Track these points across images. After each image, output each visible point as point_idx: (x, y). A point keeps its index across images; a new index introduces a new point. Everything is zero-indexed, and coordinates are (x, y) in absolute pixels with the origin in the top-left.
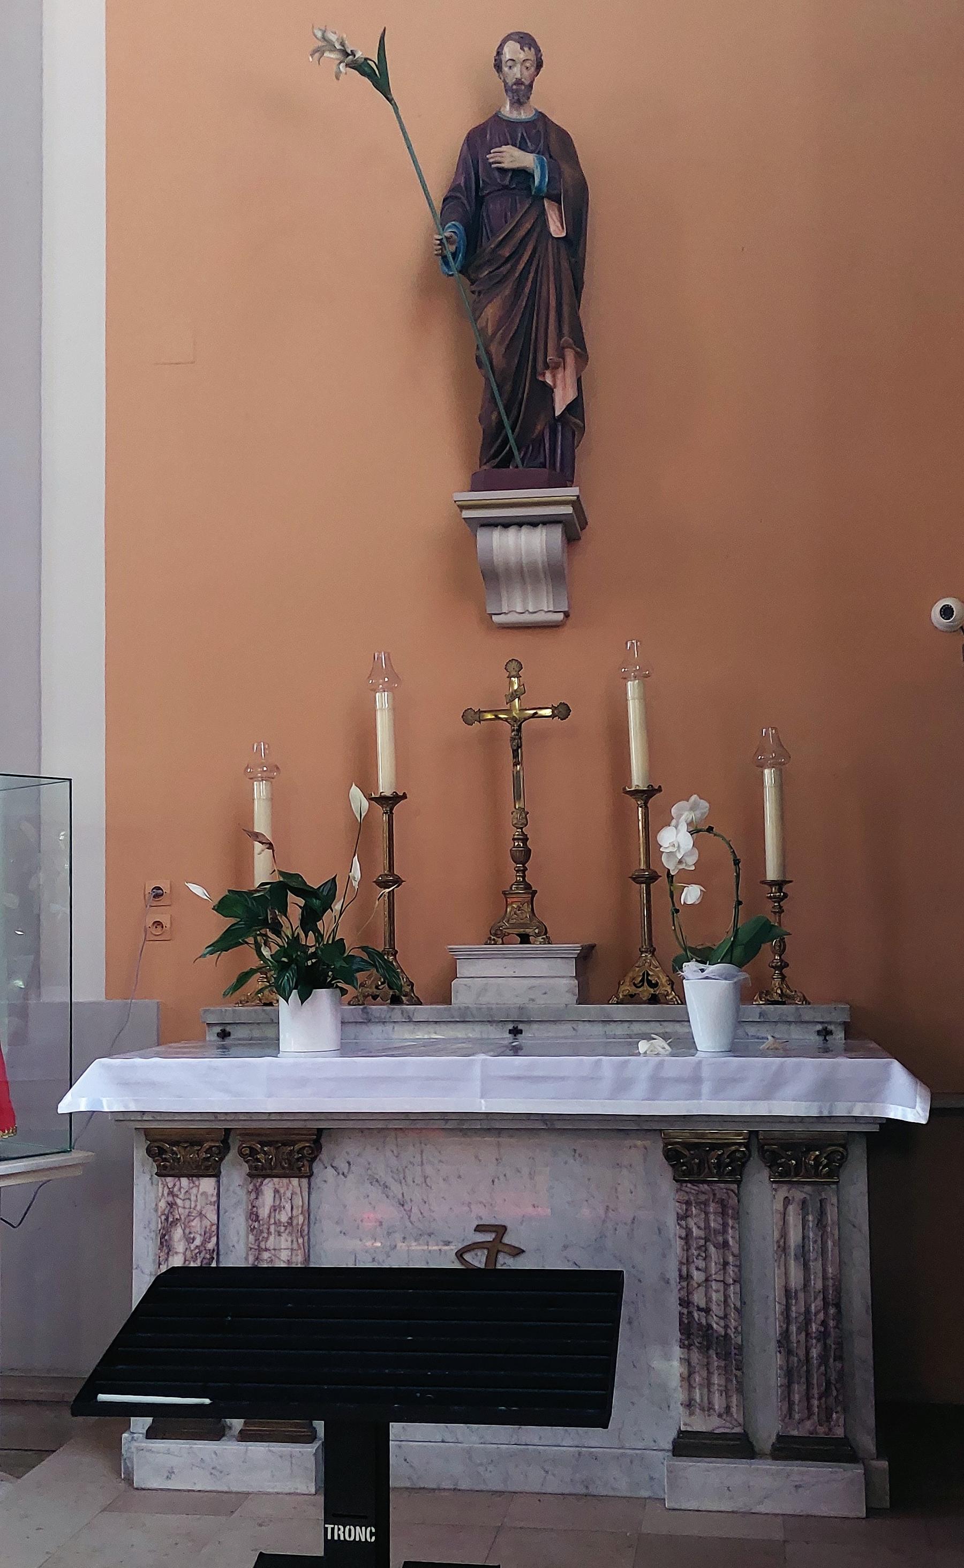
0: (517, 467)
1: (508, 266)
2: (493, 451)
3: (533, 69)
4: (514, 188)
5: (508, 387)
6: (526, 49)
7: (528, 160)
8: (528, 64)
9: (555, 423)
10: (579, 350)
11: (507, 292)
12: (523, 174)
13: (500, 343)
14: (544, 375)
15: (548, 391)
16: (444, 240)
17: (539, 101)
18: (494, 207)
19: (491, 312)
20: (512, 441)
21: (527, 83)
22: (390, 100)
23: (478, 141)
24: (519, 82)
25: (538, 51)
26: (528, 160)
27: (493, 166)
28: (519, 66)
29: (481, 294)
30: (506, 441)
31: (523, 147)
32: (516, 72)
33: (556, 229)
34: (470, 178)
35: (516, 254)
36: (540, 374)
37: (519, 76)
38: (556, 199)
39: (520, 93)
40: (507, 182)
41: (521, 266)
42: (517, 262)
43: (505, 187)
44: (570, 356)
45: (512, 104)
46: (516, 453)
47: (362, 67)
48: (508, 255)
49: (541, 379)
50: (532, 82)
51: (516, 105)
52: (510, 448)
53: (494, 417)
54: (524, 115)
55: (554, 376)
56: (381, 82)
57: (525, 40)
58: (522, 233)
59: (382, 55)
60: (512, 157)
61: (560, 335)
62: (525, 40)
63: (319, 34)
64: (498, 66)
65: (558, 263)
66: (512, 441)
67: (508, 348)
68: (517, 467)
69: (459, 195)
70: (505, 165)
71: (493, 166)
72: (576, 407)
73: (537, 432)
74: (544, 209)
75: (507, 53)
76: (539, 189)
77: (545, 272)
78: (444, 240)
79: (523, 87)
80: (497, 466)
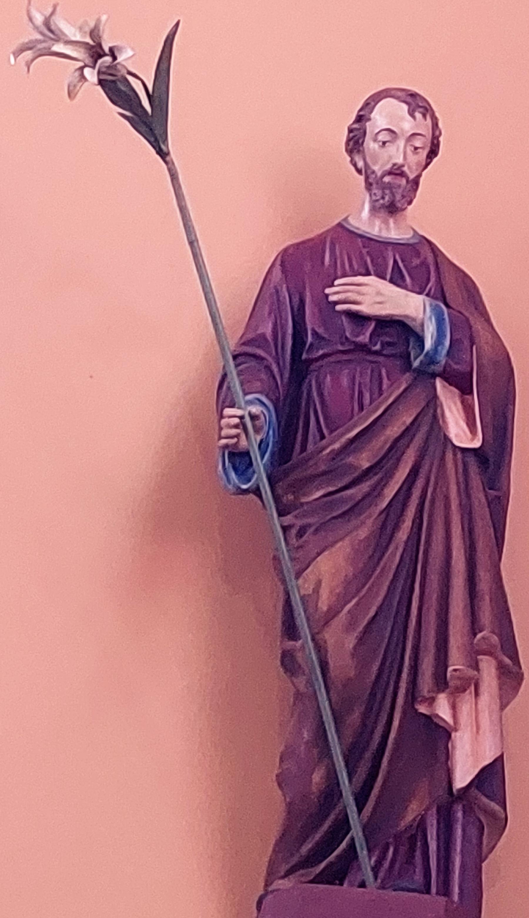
0: (363, 885)
1: (365, 487)
2: (305, 849)
3: (424, 154)
4: (376, 353)
5: (355, 717)
6: (418, 115)
7: (412, 305)
8: (418, 144)
9: (450, 802)
10: (507, 661)
11: (363, 533)
12: (398, 330)
13: (350, 626)
14: (431, 701)
15: (437, 737)
16: (248, 420)
17: (425, 218)
18: (333, 383)
19: (330, 568)
20: (356, 831)
21: (412, 176)
22: (163, 154)
23: (305, 267)
24: (397, 171)
25: (435, 125)
26: (412, 305)
27: (339, 307)
28: (401, 143)
29: (304, 539)
30: (343, 825)
31: (397, 280)
32: (396, 154)
33: (460, 431)
34: (284, 327)
35: (383, 466)
36: (425, 700)
37: (400, 160)
38: (462, 384)
39: (394, 192)
40: (364, 338)
41: (390, 492)
42: (389, 475)
43: (363, 348)
44: (488, 669)
45: (374, 210)
46: (363, 853)
47: (115, 87)
48: (366, 465)
49: (422, 709)
50: (419, 176)
51: (383, 214)
52: (352, 845)
53: (317, 777)
54: (393, 232)
55: (454, 707)
56: (150, 121)
57: (415, 103)
58: (393, 431)
59: (164, 66)
60: (378, 296)
61: (474, 627)
62: (415, 103)
63: (39, 19)
64: (355, 143)
65: (466, 491)
66: (356, 831)
67: (361, 641)
68: (363, 885)
69: (260, 352)
70: (364, 309)
71: (339, 307)
72: (491, 777)
73: (409, 817)
74: (435, 397)
75: (379, 119)
76: (431, 359)
77: (440, 504)
78: (248, 420)
79: (404, 181)
80: (317, 880)
